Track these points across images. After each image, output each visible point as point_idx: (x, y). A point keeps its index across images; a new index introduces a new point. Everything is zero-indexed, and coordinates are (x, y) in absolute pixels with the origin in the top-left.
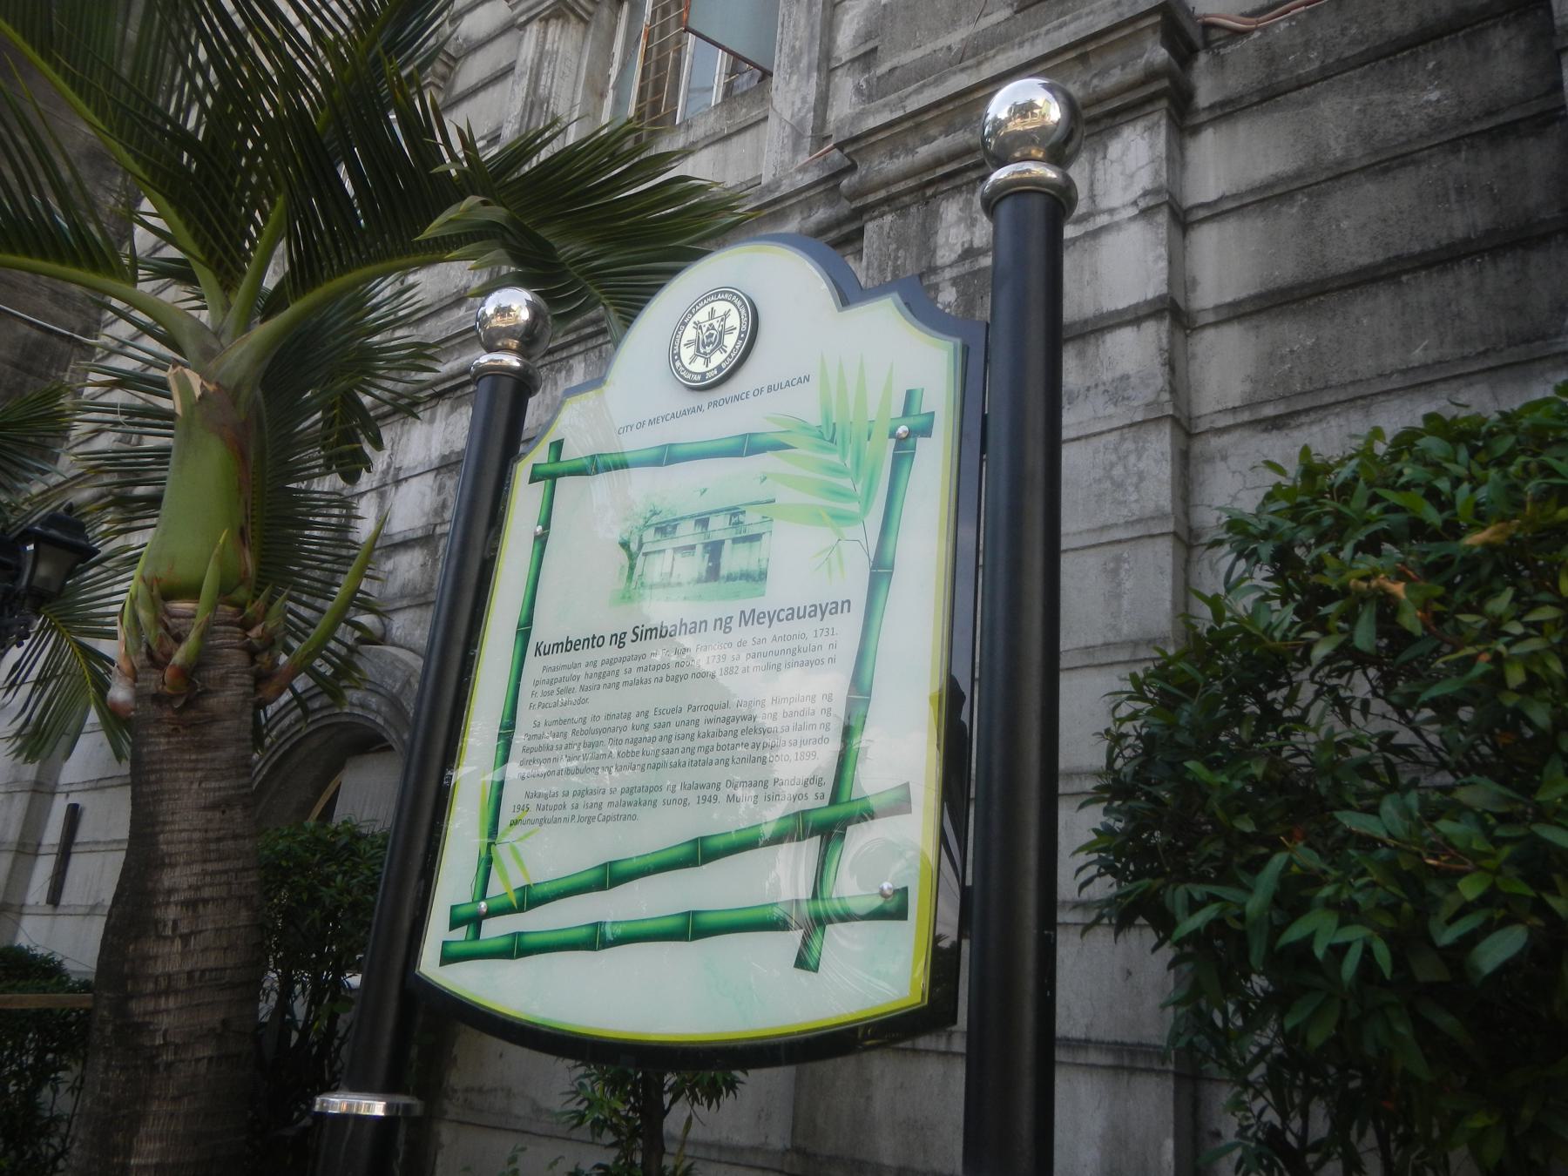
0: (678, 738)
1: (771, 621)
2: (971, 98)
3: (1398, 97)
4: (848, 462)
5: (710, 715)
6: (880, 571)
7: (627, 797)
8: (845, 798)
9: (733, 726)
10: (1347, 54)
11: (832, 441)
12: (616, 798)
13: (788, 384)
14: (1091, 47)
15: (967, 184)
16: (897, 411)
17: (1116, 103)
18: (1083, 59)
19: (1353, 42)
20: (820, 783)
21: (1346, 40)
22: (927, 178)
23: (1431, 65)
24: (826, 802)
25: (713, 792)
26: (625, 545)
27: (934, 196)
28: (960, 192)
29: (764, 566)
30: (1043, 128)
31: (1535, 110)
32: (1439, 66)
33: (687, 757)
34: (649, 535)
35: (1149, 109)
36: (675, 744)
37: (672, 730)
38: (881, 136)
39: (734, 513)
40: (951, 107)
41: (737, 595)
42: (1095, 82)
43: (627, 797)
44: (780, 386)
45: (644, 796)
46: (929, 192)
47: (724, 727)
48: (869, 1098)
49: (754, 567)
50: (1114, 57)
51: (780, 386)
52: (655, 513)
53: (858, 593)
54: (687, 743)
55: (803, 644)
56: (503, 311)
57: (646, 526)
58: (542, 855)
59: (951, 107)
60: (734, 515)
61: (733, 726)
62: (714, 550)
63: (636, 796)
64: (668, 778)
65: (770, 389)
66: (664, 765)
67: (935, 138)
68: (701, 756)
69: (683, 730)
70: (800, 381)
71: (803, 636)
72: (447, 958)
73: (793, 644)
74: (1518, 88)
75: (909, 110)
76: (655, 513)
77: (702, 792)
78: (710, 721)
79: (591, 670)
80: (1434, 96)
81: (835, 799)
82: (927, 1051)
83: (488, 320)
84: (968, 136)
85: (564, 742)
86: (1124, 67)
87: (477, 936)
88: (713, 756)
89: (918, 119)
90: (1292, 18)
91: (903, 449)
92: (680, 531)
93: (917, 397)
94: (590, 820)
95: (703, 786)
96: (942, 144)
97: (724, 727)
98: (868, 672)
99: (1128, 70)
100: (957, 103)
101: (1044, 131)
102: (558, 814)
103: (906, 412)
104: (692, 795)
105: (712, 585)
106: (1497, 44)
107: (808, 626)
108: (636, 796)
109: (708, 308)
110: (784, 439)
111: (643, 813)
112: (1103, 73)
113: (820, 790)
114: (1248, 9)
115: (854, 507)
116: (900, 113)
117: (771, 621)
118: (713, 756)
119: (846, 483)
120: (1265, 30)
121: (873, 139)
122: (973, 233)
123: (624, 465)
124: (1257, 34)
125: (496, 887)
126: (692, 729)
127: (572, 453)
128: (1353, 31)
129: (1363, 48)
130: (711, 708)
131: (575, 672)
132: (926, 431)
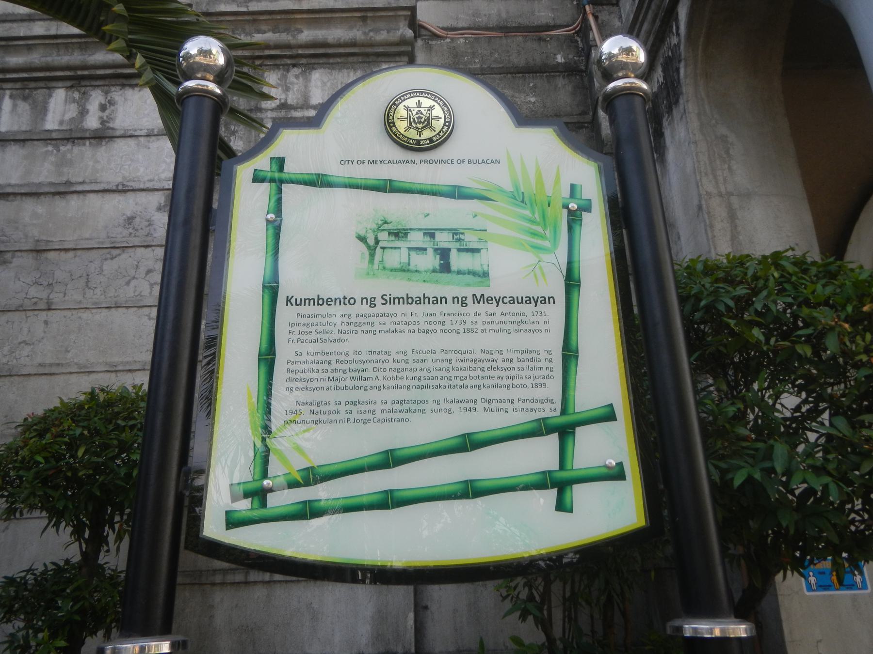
0: (435, 369)
1: (498, 303)
2: (292, 16)
3: (517, 95)
4: (537, 215)
5: (460, 357)
6: (572, 282)
7: (398, 407)
8: (571, 411)
9: (480, 365)
10: (493, 66)
11: (523, 202)
12: (388, 407)
13: (483, 161)
14: (370, 14)
15: (283, 65)
16: (566, 193)
17: (381, 50)
18: (364, 19)
19: (495, 61)
20: (552, 402)
21: (493, 59)
22: (257, 53)
23: (531, 85)
24: (558, 413)
25: (472, 405)
26: (362, 239)
27: (261, 65)
28: (279, 69)
29: (486, 269)
30: (636, 63)
31: (576, 120)
32: (535, 87)
33: (446, 382)
34: (383, 236)
35: (397, 59)
36: (433, 374)
37: (429, 364)
38: (228, 18)
39: (456, 233)
40: (279, 17)
41: (468, 285)
42: (371, 34)
43: (398, 407)
44: (477, 161)
45: (413, 407)
46: (258, 62)
47: (473, 365)
48: (212, 617)
49: (478, 268)
50: (381, 24)
51: (477, 161)
52: (386, 223)
53: (558, 290)
54: (444, 373)
55: (524, 319)
56: (206, 53)
57: (379, 229)
58: (304, 444)
59: (279, 17)
60: (457, 234)
61: (480, 365)
62: (444, 254)
63: (406, 406)
64: (429, 394)
65: (470, 161)
66: (427, 387)
67: (264, 32)
68: (454, 382)
69: (438, 365)
70: (492, 161)
71: (523, 314)
72: (233, 522)
73: (517, 318)
74: (569, 108)
75: (251, 9)
76: (386, 223)
77: (463, 405)
78: (461, 361)
79: (346, 320)
80: (533, 100)
81: (564, 412)
82: (255, 583)
83: (191, 56)
84: (290, 38)
85: (330, 368)
86: (388, 32)
87: (264, 504)
88: (468, 382)
89: (255, 17)
90: (466, 38)
91: (574, 218)
92: (412, 236)
93: (578, 189)
94: (365, 421)
95: (462, 401)
96: (269, 37)
97: (473, 365)
98: (573, 338)
99: (391, 34)
100: (283, 16)
101: (636, 64)
102: (332, 417)
103: (572, 194)
104: (455, 407)
105: (445, 276)
106: (560, 85)
107: (528, 309)
108: (406, 406)
109: (432, 103)
110: (485, 194)
111: (414, 417)
112: (377, 31)
113: (553, 406)
114: (441, 26)
115: (547, 244)
116: (244, 9)
117: (498, 303)
118: (468, 382)
119: (539, 229)
120: (452, 39)
121: (222, 18)
122: (287, 95)
123: (330, 185)
124: (448, 40)
125: (276, 468)
126: (446, 365)
127: (290, 168)
128: (496, 56)
129: (501, 66)
130: (460, 352)
131: (331, 320)
132: (588, 209)
